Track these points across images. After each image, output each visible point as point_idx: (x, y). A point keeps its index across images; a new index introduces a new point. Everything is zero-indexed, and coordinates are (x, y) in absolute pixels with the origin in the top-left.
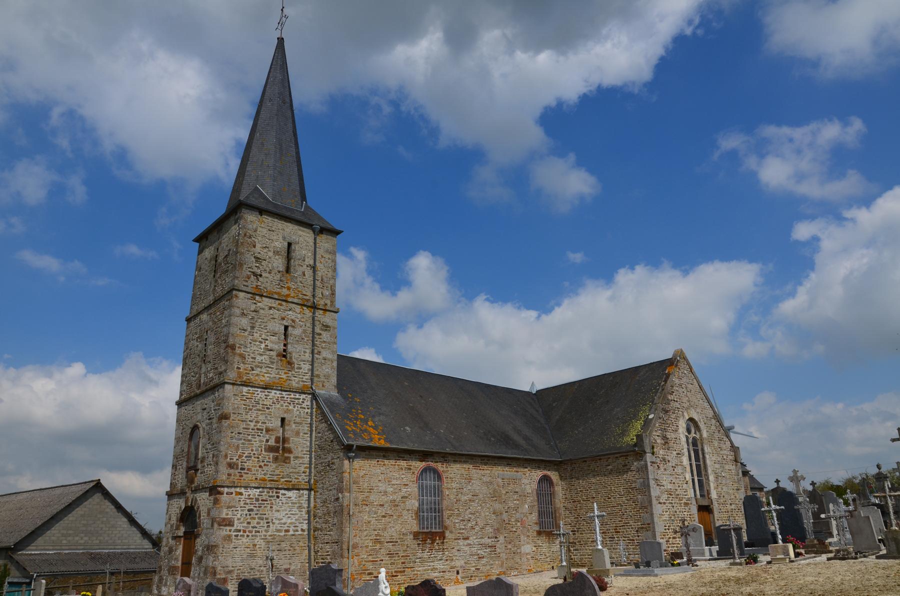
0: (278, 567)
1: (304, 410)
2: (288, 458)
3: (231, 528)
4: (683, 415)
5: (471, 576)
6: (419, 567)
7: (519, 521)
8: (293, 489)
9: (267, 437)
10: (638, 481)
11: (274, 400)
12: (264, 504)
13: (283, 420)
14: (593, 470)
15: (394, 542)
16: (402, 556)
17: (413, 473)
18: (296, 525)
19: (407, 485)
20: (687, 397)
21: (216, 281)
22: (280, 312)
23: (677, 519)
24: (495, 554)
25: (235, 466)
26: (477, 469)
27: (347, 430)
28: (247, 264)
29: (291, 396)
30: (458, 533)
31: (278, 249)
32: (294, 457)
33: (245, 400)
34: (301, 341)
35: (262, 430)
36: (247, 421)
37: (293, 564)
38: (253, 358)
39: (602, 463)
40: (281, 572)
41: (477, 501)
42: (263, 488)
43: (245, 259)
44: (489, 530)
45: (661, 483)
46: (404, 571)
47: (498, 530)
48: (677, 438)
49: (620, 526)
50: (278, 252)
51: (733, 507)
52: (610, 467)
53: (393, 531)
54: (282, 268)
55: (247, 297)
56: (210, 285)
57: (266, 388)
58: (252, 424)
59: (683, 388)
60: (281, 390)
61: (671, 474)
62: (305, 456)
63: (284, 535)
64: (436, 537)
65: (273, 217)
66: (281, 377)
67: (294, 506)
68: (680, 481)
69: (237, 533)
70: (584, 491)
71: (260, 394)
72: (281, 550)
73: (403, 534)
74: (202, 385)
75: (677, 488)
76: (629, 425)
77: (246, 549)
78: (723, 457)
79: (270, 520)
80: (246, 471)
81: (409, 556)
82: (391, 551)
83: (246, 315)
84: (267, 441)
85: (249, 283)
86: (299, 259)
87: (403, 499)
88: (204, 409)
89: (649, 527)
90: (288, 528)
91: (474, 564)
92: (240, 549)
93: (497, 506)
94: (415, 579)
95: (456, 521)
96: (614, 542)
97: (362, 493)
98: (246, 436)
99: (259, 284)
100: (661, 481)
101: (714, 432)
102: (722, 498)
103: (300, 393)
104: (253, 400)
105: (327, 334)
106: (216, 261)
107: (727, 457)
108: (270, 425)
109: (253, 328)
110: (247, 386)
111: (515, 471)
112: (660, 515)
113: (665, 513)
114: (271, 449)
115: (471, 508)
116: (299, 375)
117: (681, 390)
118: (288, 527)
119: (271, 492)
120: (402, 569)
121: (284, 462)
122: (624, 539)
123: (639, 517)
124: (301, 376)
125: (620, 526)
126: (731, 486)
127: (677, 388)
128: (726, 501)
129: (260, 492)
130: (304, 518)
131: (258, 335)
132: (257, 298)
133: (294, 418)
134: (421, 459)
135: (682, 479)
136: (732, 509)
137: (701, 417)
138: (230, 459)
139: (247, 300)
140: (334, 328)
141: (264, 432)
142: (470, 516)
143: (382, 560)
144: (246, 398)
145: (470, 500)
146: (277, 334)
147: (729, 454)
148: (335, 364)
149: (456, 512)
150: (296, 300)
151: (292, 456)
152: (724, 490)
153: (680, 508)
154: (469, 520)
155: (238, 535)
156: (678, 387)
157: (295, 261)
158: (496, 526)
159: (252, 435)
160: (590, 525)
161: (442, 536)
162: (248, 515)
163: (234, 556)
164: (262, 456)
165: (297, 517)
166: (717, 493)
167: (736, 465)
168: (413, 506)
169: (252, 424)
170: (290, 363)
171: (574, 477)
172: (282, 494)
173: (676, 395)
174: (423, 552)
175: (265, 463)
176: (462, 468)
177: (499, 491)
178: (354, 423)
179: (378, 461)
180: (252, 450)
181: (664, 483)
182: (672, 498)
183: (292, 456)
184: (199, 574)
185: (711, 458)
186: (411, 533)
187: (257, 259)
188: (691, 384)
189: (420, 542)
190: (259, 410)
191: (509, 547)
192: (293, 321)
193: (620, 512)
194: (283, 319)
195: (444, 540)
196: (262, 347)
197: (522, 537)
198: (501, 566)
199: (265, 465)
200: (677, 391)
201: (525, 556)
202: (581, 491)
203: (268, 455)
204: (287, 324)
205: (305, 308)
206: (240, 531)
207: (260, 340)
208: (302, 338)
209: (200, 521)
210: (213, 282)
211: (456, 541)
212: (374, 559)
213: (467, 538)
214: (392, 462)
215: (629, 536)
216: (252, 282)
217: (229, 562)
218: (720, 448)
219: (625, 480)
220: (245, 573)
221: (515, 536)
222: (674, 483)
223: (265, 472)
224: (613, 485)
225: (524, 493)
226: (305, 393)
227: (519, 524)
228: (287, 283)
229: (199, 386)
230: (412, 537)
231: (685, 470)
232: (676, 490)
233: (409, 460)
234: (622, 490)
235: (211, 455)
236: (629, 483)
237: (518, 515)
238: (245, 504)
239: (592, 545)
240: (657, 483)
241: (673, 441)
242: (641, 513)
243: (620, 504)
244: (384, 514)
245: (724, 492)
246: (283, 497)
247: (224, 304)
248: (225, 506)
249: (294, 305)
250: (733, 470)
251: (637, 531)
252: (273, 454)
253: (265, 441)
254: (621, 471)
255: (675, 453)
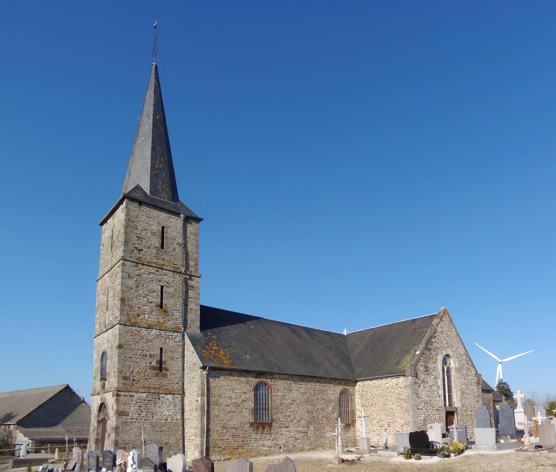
0: (160, 441)
1: (176, 343)
2: (166, 374)
3: (127, 417)
4: (442, 353)
5: (290, 450)
6: (254, 444)
7: (325, 417)
8: (170, 394)
9: (151, 360)
10: (405, 394)
11: (155, 336)
12: (150, 403)
13: (161, 349)
14: (376, 386)
15: (236, 428)
16: (242, 437)
17: (250, 385)
18: (172, 416)
19: (246, 393)
20: (446, 340)
21: (113, 254)
22: (157, 276)
23: (430, 419)
24: (307, 437)
25: (129, 379)
26: (296, 384)
27: (204, 357)
28: (131, 241)
29: (167, 334)
30: (282, 424)
31: (155, 231)
32: (169, 374)
33: (133, 336)
34: (173, 297)
35: (147, 356)
36: (135, 350)
37: (171, 440)
38: (138, 308)
39: (383, 382)
40: (163, 444)
41: (295, 404)
42: (148, 393)
43: (129, 238)
44: (303, 422)
45: (421, 396)
46: (243, 446)
47: (309, 422)
48: (435, 368)
49: (391, 423)
50: (155, 233)
51: (472, 413)
52: (387, 385)
53: (235, 422)
54: (158, 245)
55: (132, 265)
56: (109, 256)
57: (148, 328)
58: (139, 352)
59: (443, 334)
60: (160, 330)
61: (428, 391)
62: (178, 373)
63: (164, 422)
64: (266, 426)
65: (150, 207)
66: (160, 321)
67: (171, 405)
68: (435, 395)
69: (132, 420)
70: (370, 400)
71: (144, 332)
72: (162, 432)
73: (243, 424)
74: (107, 325)
75: (432, 400)
76: (403, 358)
77: (138, 430)
78: (469, 380)
79: (154, 413)
80: (136, 382)
81: (247, 437)
82: (234, 434)
83: (132, 278)
84: (151, 363)
85: (133, 255)
86: (171, 239)
87: (243, 402)
88: (108, 341)
89: (410, 424)
90: (167, 418)
91: (292, 443)
92: (134, 430)
93: (310, 407)
94: (251, 451)
95: (280, 416)
96: (387, 432)
97: (214, 398)
98: (135, 359)
99: (141, 256)
100: (421, 395)
101: (464, 364)
102: (465, 406)
103: (173, 332)
104: (139, 336)
105: (192, 293)
106: (112, 239)
107: (472, 381)
108: (152, 353)
109: (137, 287)
110: (134, 326)
111: (323, 386)
112: (417, 416)
113: (421, 415)
114: (153, 368)
115: (291, 408)
116: (172, 320)
117: (442, 335)
118: (167, 417)
119: (154, 396)
120: (242, 445)
121: (163, 376)
122: (394, 430)
123: (403, 417)
124: (173, 321)
125: (391, 423)
126: (473, 399)
127: (439, 334)
128: (467, 409)
129: (146, 395)
130: (178, 412)
131: (142, 292)
132: (140, 266)
133: (170, 348)
134: (256, 376)
135: (436, 394)
136: (471, 414)
137: (455, 354)
138: (125, 374)
139: (132, 267)
140: (198, 288)
141: (148, 357)
142: (290, 413)
143: (228, 439)
144: (134, 334)
145: (290, 404)
146: (156, 291)
147: (473, 378)
148: (199, 313)
149: (280, 410)
150: (168, 268)
151: (168, 373)
152: (467, 402)
153: (433, 412)
154: (290, 416)
155: (132, 421)
156: (440, 333)
157: (167, 240)
158: (308, 420)
159: (140, 359)
160: (373, 421)
161: (270, 425)
162: (139, 409)
163: (130, 434)
164: (147, 372)
165: (173, 411)
166: (461, 404)
167: (478, 386)
168: (250, 406)
169: (139, 352)
170: (166, 312)
171: (364, 390)
172: (162, 397)
173: (437, 339)
174: (257, 434)
175: (149, 377)
176: (285, 383)
177: (311, 398)
178: (209, 352)
179: (225, 378)
180: (140, 369)
181: (423, 396)
182: (428, 406)
183: (168, 373)
184: (109, 444)
185: (459, 381)
186: (248, 423)
187: (139, 238)
188: (450, 331)
189: (255, 429)
190: (144, 343)
191: (317, 433)
192: (167, 283)
193: (392, 413)
194: (160, 281)
195: (271, 427)
196: (145, 300)
197: (326, 427)
198: (311, 444)
199: (149, 378)
200: (439, 336)
201: (327, 439)
202: (368, 399)
203: (151, 372)
204: (162, 285)
205: (176, 274)
206: (133, 419)
207: (143, 295)
208: (174, 295)
209: (108, 412)
210: (111, 254)
211: (280, 429)
212: (222, 439)
213: (288, 427)
214: (236, 378)
215: (397, 429)
216: (135, 254)
217: (127, 438)
218: (467, 374)
219: (397, 393)
220: (138, 444)
221: (321, 427)
222: (430, 396)
223: (150, 382)
224: (389, 397)
225: (329, 399)
226: (177, 332)
227: (324, 419)
228: (162, 256)
229: (105, 326)
230: (249, 425)
231: (439, 388)
232: (431, 401)
233: (247, 377)
234: (394, 400)
235: (113, 371)
236: (399, 395)
237: (324, 414)
238: (136, 402)
239: (373, 433)
240: (418, 396)
241: (432, 369)
242: (405, 415)
243: (392, 409)
244: (229, 411)
245: (467, 403)
246: (163, 398)
247: (117, 269)
248: (122, 404)
249: (167, 272)
250: (475, 389)
251: (402, 426)
252: (156, 371)
253: (149, 363)
254: (394, 387)
255: (433, 377)
